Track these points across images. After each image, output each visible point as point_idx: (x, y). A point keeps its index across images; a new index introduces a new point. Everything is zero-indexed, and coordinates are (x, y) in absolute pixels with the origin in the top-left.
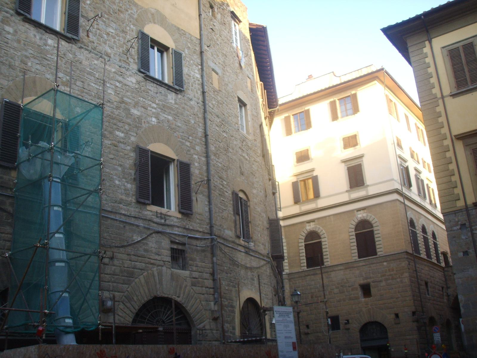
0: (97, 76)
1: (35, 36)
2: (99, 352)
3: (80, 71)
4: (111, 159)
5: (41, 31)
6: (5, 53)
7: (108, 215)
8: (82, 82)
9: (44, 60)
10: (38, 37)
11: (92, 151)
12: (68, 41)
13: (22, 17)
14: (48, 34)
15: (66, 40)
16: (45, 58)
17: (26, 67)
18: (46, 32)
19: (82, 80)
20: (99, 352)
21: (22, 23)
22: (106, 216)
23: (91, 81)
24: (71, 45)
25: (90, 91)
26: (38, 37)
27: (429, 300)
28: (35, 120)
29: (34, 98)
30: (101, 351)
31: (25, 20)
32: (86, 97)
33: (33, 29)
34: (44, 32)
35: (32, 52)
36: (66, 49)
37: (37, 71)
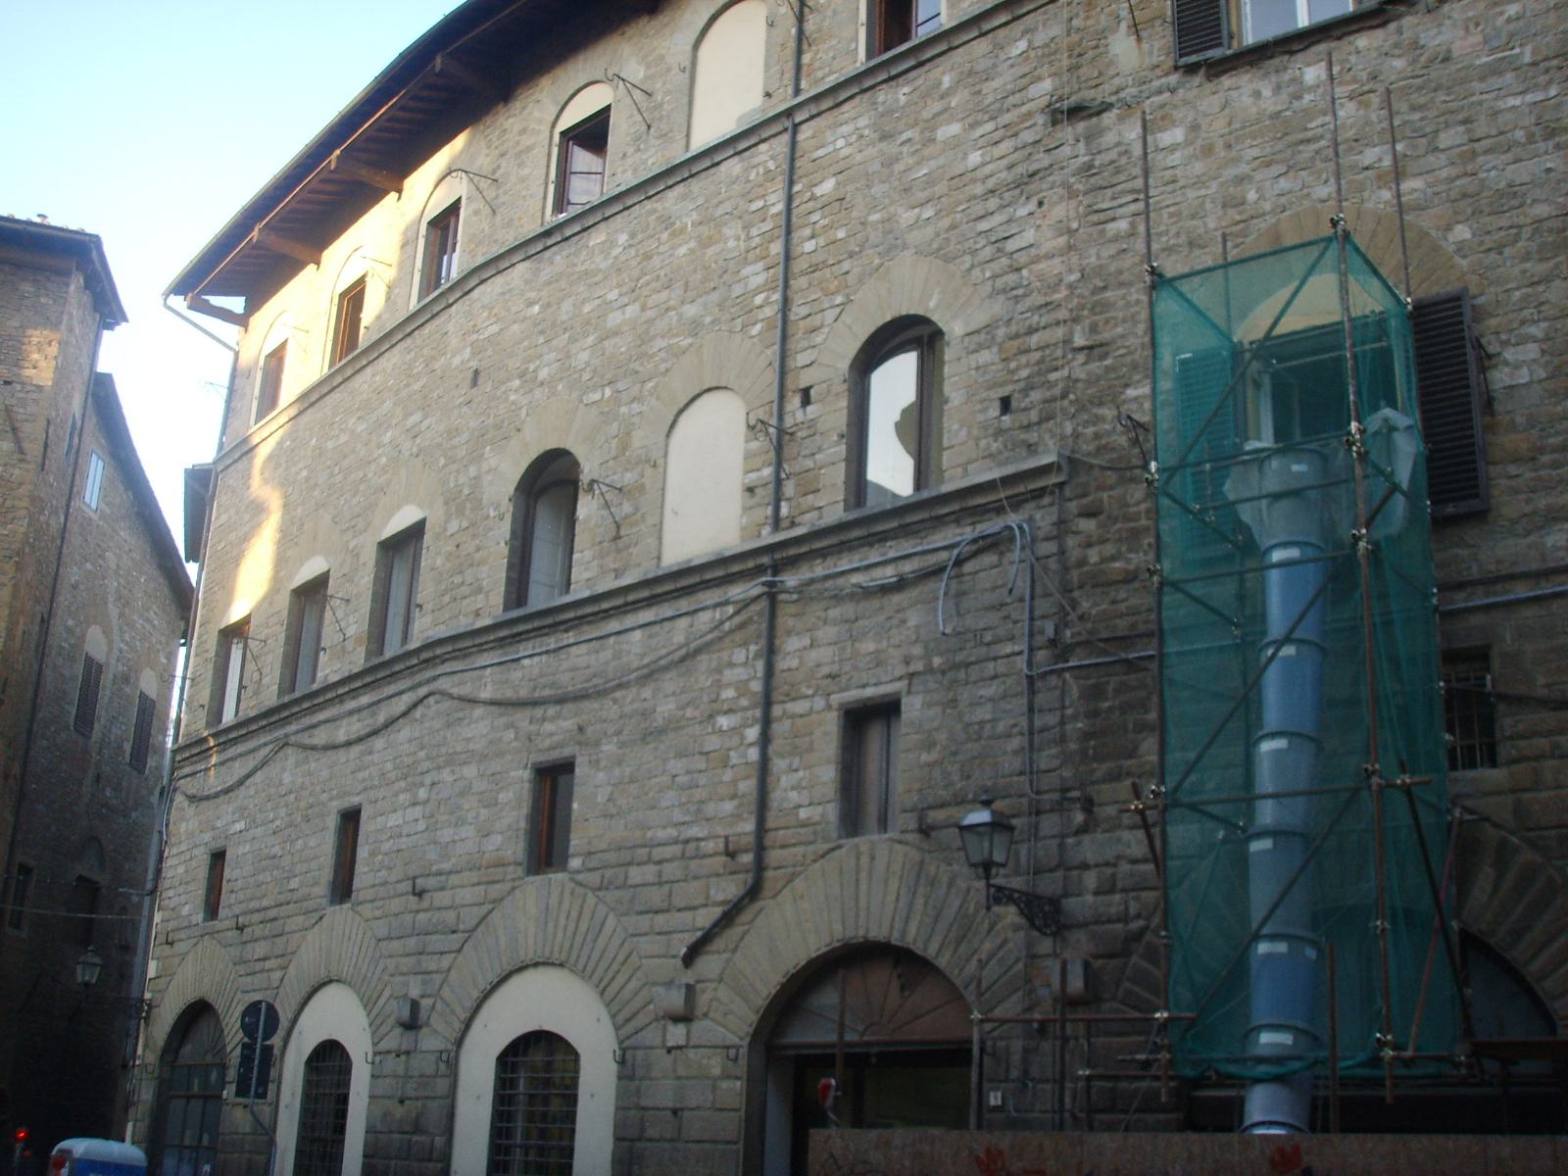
0: (1527, 58)
1: (1257, 94)
2: (982, 1155)
3: (1449, 89)
4: (726, 388)
5: (1276, 61)
6: (1171, 215)
7: (1507, 592)
8: (1465, 122)
9: (1301, 147)
10: (1267, 92)
11: (1543, 352)
12: (1374, 23)
13: (1202, 72)
14: (1300, 56)
15: (1368, 24)
16: (1302, 142)
17: (1240, 213)
18: (1292, 53)
19: (1460, 117)
20: (982, 1155)
21: (1209, 87)
22: (1499, 599)
23: (1502, 92)
24: (1392, 26)
25: (1502, 133)
26: (1267, 92)
27: (1117, 93)
28: (1308, 360)
29: (1284, 293)
30: (988, 1151)
31: (1212, 72)
32: (1490, 165)
33: (1249, 76)
34: (1287, 57)
35: (1255, 152)
36: (1374, 55)
37: (1283, 200)
